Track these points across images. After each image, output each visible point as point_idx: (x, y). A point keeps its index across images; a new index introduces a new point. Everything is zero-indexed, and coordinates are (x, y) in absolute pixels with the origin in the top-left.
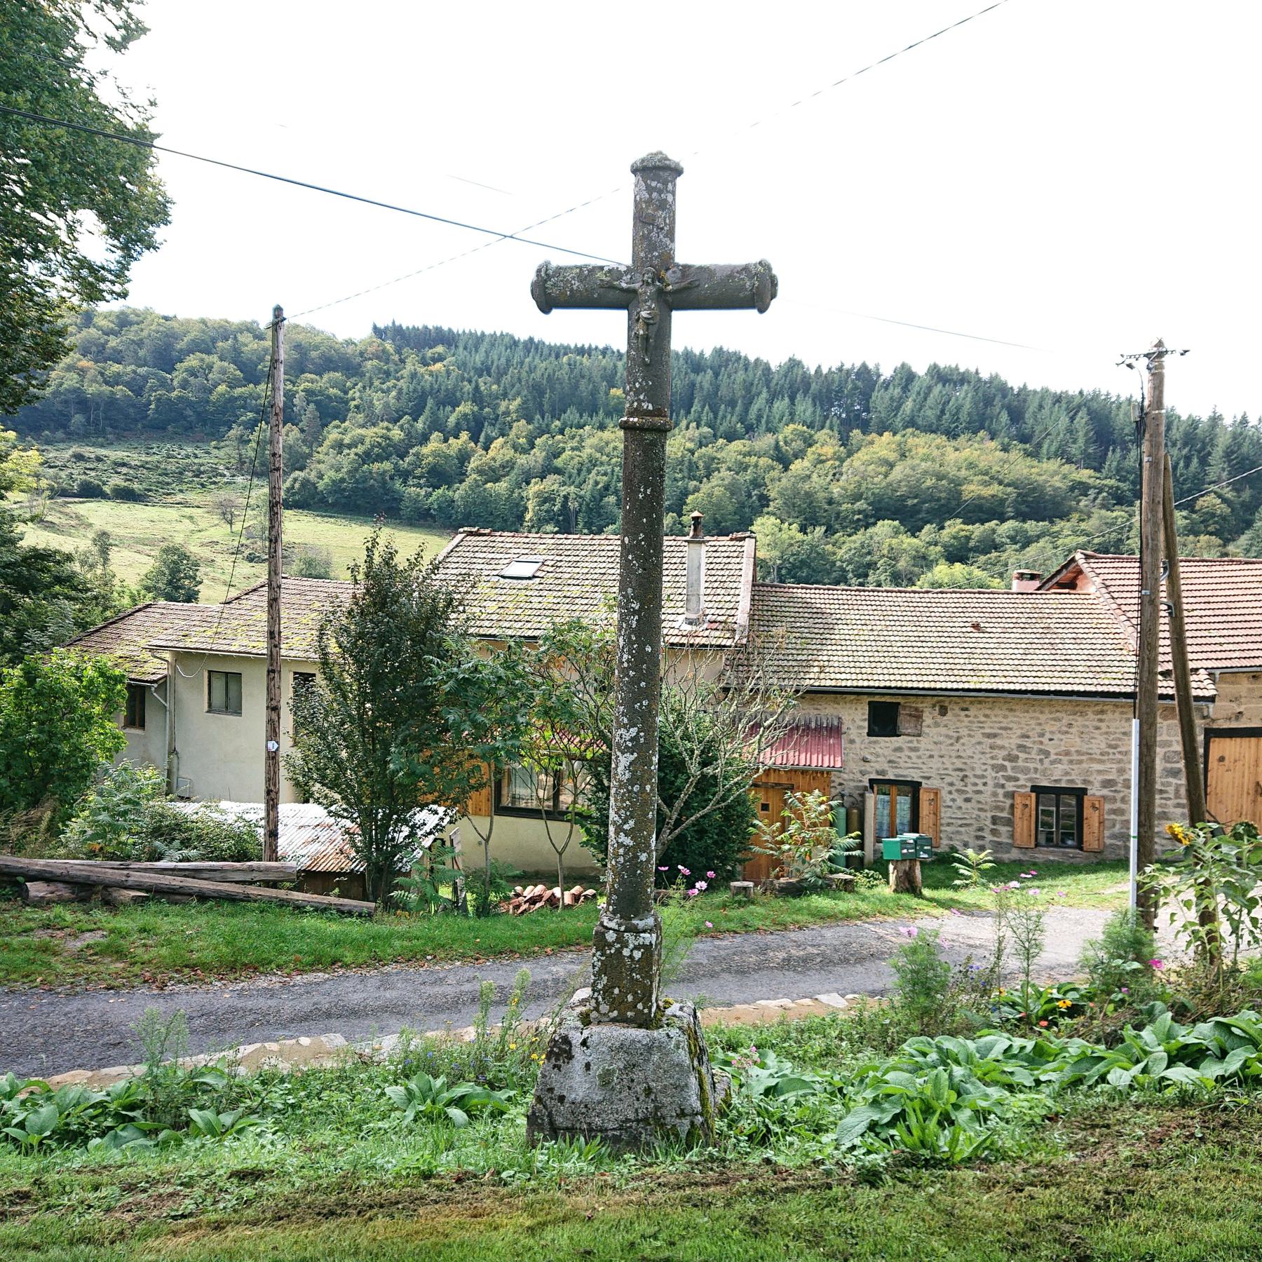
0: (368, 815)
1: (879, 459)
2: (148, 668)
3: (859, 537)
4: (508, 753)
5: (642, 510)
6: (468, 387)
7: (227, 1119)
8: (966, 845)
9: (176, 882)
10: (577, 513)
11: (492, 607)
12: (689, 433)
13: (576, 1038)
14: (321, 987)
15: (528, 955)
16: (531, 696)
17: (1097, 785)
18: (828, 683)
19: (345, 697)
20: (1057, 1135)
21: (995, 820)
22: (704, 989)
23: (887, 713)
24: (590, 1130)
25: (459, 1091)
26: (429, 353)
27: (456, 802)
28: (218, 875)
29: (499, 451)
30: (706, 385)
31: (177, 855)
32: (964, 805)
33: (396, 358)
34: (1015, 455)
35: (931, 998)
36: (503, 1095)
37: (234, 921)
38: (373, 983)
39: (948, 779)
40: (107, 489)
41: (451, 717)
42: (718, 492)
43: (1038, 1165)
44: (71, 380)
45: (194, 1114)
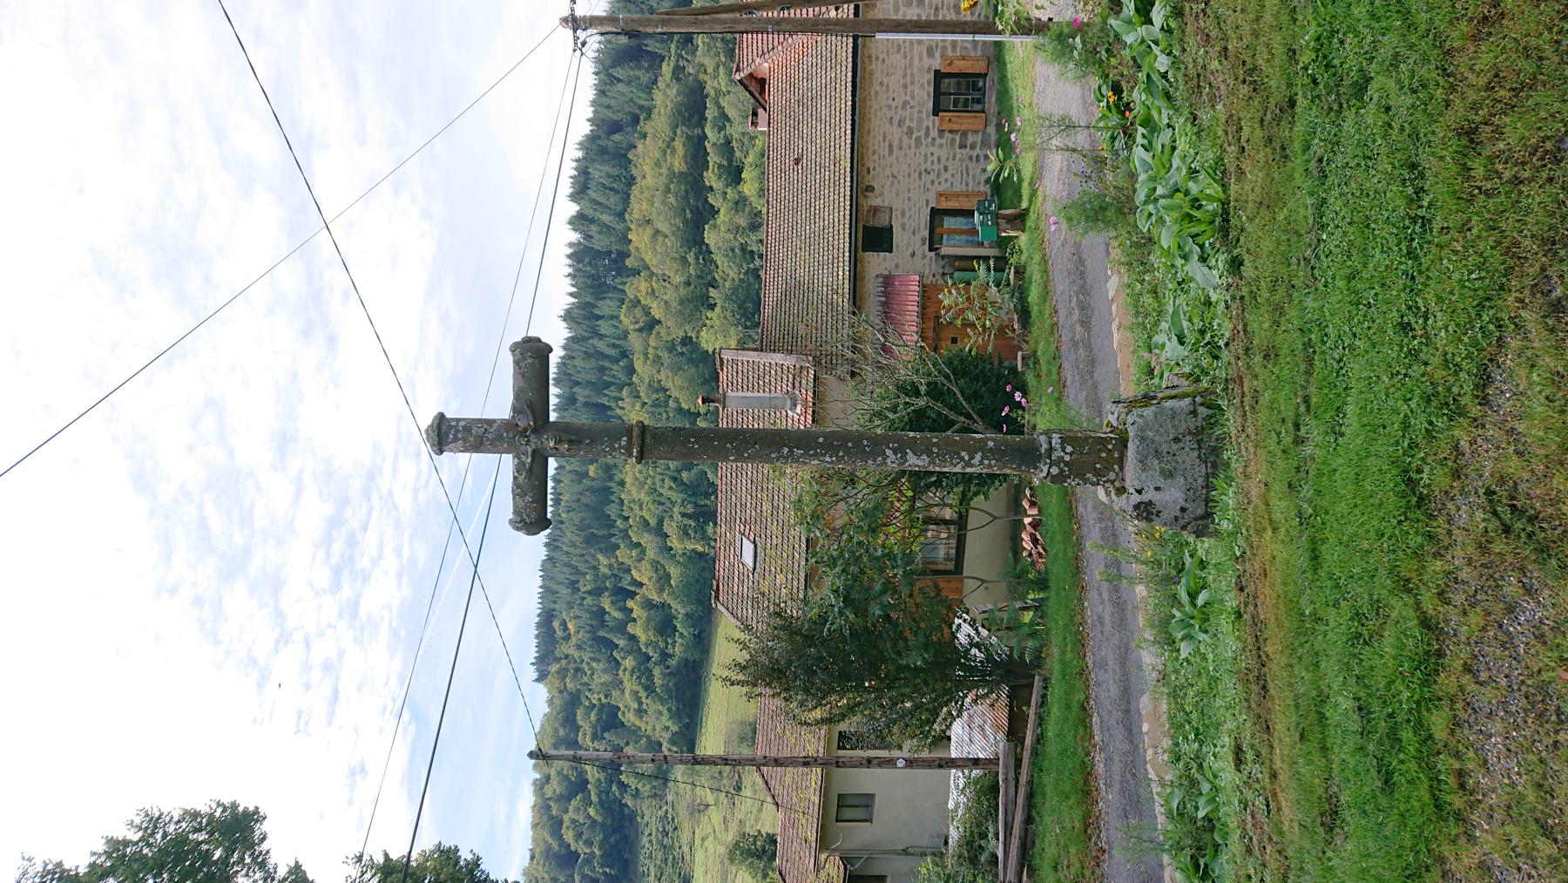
0: (961, 684)
1: (651, 238)
2: (834, 873)
4: (908, 564)
5: (696, 445)
6: (589, 600)
7: (1205, 787)
8: (984, 170)
10: (696, 505)
11: (780, 578)
12: (628, 407)
15: (1079, 544)
16: (860, 543)
17: (931, 61)
19: (860, 703)
20: (1204, 116)
21: (962, 146)
22: (1106, 396)
23: (873, 236)
25: (1184, 597)
26: (559, 633)
27: (949, 608)
28: (1010, 808)
29: (643, 573)
31: (993, 842)
32: (950, 171)
34: (648, 127)
35: (1106, 209)
36: (1188, 560)
37: (1049, 793)
38: (1102, 676)
39: (929, 185)
41: (878, 612)
43: (1226, 133)
45: (1201, 814)
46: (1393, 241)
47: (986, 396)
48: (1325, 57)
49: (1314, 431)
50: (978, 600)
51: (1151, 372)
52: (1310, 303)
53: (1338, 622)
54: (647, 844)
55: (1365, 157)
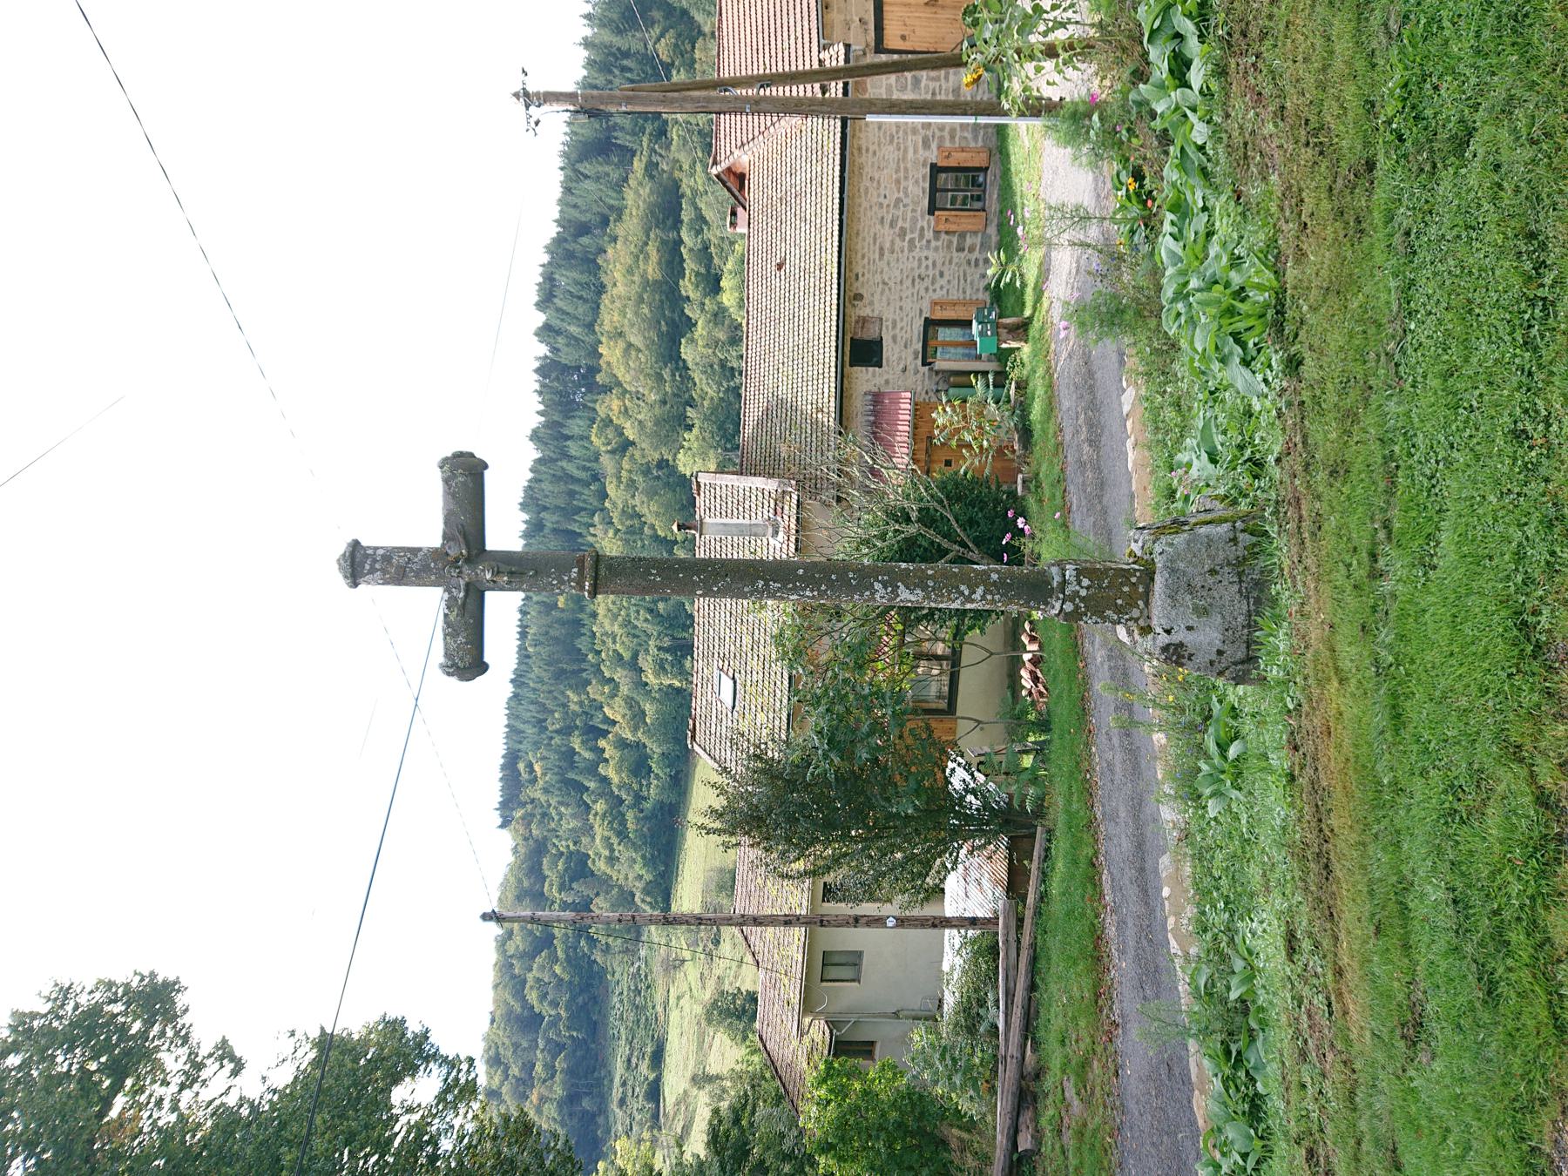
0: (956, 833)
1: (622, 356)
3: (697, 376)
4: (897, 703)
5: (673, 578)
6: (557, 740)
7: (1238, 965)
8: (984, 276)
9: (1018, 1012)
11: (761, 717)
12: (600, 533)
13: (1164, 639)
14: (1115, 880)
15: (1086, 684)
16: (845, 681)
17: (927, 153)
18: (832, 404)
19: (846, 854)
20: (1254, 191)
21: (960, 249)
23: (860, 350)
24: (1249, 626)
25: (1212, 748)
26: (525, 776)
28: (1011, 973)
30: (555, 518)
31: (993, 1011)
32: (946, 277)
33: (529, 807)
34: (620, 230)
35: (1123, 309)
36: (1216, 707)
37: (1054, 958)
38: (1112, 829)
39: (922, 293)
40: (652, 1077)
41: (865, 756)
42: (654, 508)
43: (1282, 209)
44: (550, 1110)
45: (1234, 995)
46: (1503, 330)
47: (982, 522)
48: (1413, 107)
49: (1396, 563)
50: (973, 742)
51: (1171, 494)
52: (1392, 407)
53: (1425, 796)
54: (618, 1004)
55: (1468, 227)
